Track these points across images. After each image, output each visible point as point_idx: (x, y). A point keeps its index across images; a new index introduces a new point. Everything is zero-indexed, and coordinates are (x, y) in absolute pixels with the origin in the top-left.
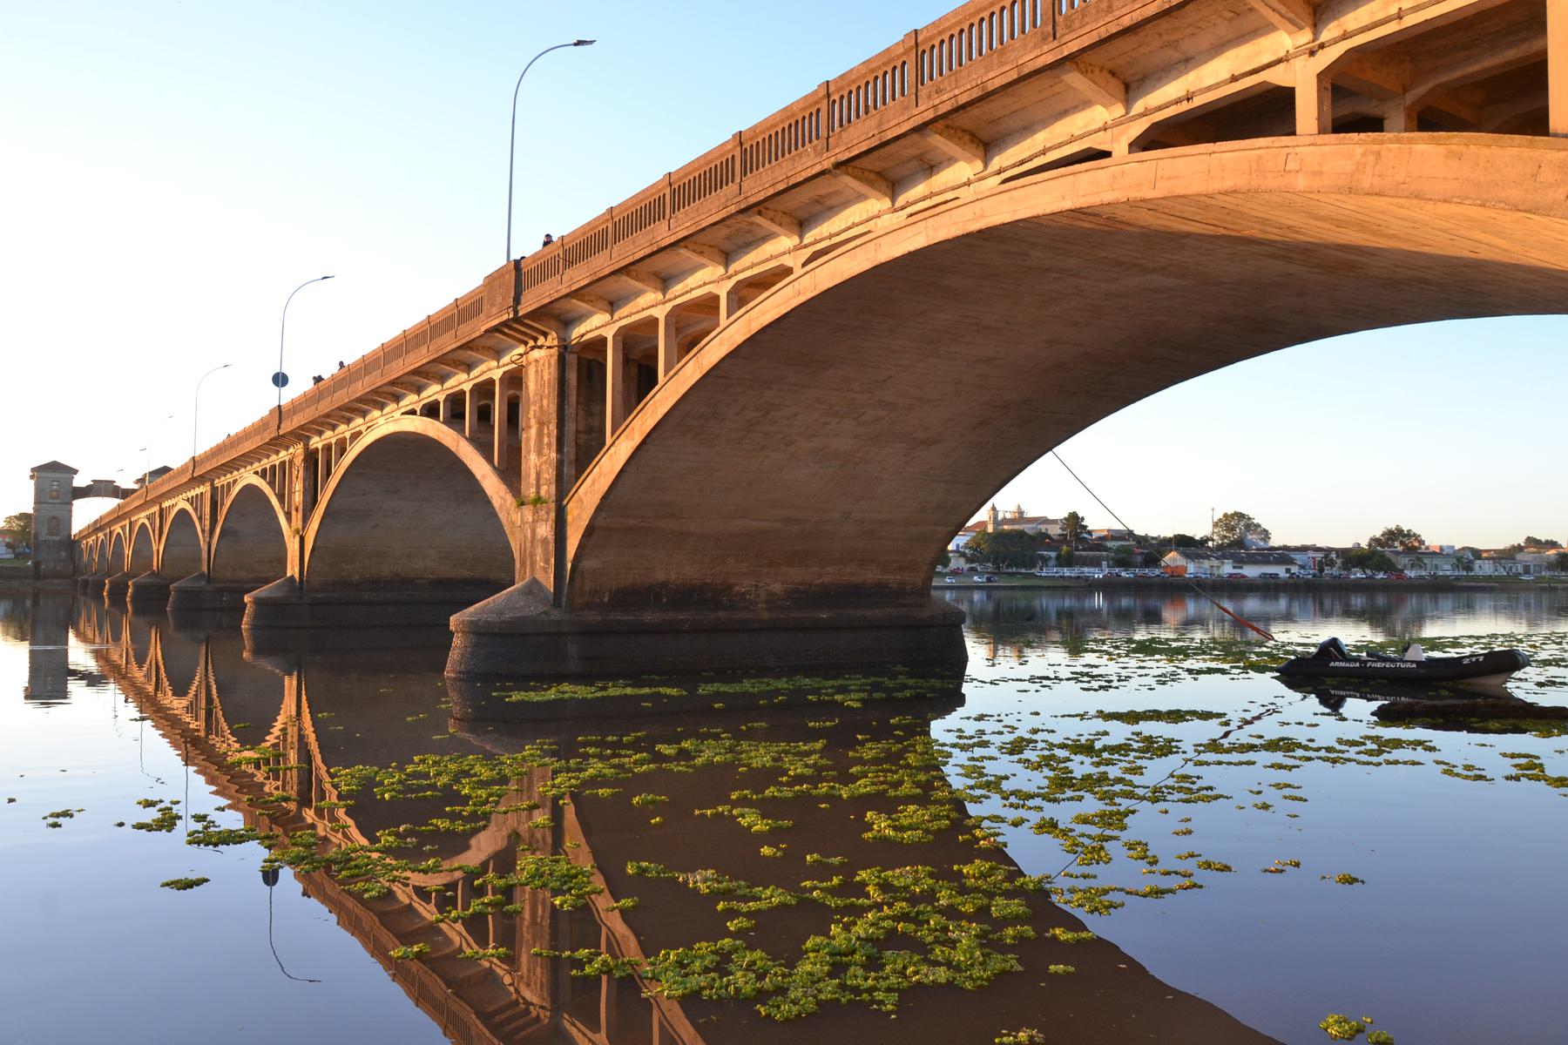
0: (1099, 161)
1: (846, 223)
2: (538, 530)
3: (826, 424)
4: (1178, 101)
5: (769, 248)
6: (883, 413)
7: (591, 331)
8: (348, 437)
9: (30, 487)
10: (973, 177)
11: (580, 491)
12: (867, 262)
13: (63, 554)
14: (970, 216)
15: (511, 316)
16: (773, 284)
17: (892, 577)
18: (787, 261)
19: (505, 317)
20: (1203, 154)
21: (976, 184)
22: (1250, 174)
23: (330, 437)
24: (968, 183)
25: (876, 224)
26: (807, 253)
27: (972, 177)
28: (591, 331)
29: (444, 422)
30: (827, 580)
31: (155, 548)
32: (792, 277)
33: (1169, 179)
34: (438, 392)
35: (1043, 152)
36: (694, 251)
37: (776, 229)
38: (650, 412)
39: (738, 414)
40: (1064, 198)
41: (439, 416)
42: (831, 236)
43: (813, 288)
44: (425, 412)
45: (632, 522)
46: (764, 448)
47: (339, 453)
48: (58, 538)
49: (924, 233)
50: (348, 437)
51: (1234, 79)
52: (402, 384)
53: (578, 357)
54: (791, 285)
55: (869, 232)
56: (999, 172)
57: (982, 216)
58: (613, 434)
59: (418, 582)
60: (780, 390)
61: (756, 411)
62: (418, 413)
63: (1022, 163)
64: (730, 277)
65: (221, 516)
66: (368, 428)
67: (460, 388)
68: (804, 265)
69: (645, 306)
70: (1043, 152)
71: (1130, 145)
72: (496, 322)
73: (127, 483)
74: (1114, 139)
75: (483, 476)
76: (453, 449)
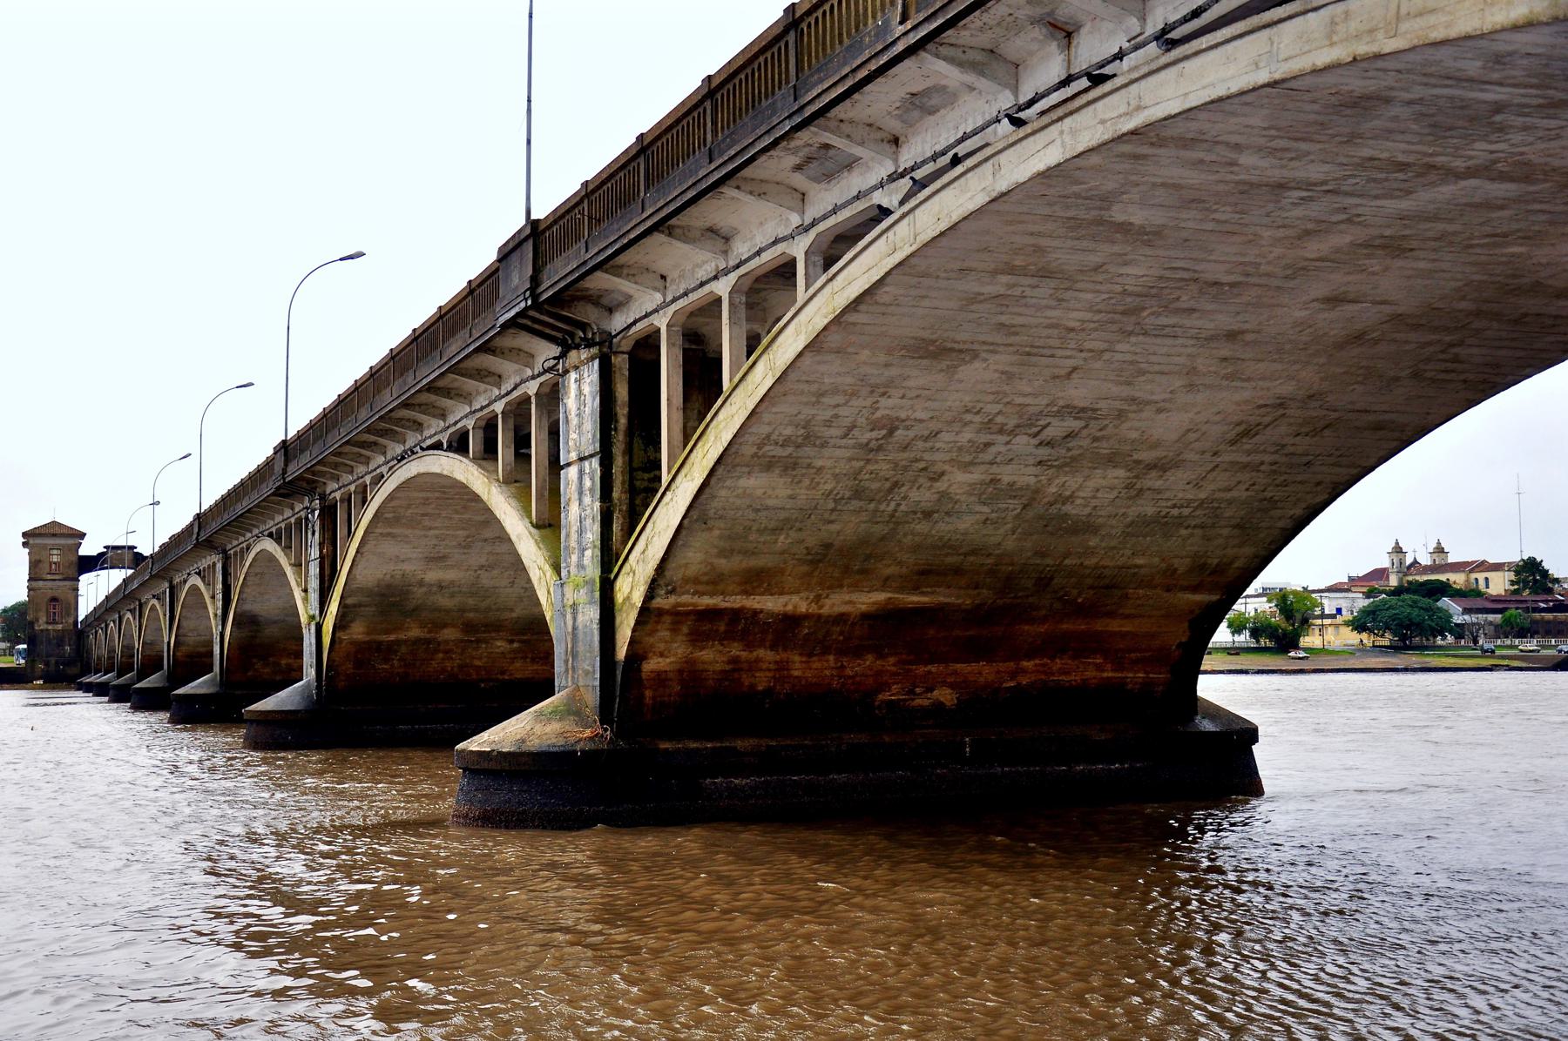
1: (956, 133)
2: (580, 618)
3: (987, 445)
5: (856, 182)
6: (1077, 424)
8: (470, 427)
10: (1128, 44)
11: (631, 557)
12: (981, 194)
14: (1123, 109)
16: (861, 237)
17: (1131, 675)
18: (879, 198)
19: (523, 305)
21: (1132, 55)
25: (995, 133)
27: (1126, 45)
29: (474, 460)
31: (166, 640)
33: (1420, 14)
36: (751, 193)
37: (857, 151)
38: (713, 439)
39: (845, 436)
40: (1257, 67)
41: (468, 452)
43: (912, 240)
44: (455, 444)
47: (679, 437)
48: (60, 627)
49: (1058, 142)
50: (470, 427)
52: (420, 405)
54: (885, 236)
55: (987, 145)
57: (1139, 108)
61: (872, 430)
62: (445, 446)
63: (1196, 14)
64: (806, 230)
65: (350, 534)
66: (390, 469)
68: (902, 203)
69: (704, 279)
75: (519, 536)
76: (485, 497)
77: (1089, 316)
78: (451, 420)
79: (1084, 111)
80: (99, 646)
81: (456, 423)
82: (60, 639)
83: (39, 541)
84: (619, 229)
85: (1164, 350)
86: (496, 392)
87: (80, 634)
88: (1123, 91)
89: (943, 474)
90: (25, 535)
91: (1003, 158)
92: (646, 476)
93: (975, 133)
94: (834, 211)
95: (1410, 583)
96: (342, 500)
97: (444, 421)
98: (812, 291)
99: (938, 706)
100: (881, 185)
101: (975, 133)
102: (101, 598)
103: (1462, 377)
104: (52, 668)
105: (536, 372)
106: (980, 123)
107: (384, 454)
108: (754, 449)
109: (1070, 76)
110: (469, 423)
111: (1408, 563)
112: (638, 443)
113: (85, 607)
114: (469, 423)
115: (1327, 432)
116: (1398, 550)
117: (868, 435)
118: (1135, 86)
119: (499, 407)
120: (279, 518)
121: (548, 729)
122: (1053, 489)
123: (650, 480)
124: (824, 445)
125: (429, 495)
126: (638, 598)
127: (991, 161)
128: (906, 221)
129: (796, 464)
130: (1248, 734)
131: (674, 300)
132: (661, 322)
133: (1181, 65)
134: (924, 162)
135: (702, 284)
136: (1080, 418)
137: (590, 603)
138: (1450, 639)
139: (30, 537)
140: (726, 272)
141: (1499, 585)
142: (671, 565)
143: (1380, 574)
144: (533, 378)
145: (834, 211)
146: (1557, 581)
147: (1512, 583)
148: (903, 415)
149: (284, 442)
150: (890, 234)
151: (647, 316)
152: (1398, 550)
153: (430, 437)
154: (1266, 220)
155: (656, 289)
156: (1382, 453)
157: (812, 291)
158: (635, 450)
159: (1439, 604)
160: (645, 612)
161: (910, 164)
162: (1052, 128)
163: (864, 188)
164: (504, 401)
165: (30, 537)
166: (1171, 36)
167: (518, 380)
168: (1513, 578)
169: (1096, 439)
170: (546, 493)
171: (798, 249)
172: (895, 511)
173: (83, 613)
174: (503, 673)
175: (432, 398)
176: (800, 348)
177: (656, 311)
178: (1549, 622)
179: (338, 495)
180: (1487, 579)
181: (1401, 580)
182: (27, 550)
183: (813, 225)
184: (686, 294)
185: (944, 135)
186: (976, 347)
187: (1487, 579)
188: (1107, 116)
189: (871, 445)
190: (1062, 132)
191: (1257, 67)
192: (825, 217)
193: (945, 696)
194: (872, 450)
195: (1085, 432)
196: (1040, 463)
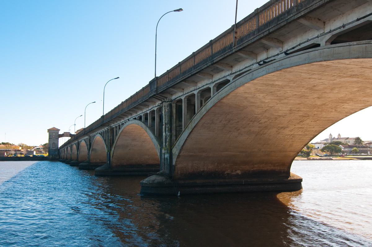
0: (316, 48)
2: (165, 156)
4: (340, 28)
7: (178, 97)
8: (142, 115)
9: (47, 135)
13: (56, 153)
15: (156, 93)
17: (277, 168)
18: (228, 78)
19: (154, 94)
20: (348, 46)
22: (363, 52)
23: (193, 89)
24: (278, 55)
25: (252, 67)
26: (234, 76)
27: (279, 53)
28: (178, 97)
29: (143, 122)
30: (255, 169)
32: (229, 83)
34: (141, 113)
35: (299, 45)
39: (220, 122)
42: (240, 71)
45: (191, 154)
46: (230, 131)
48: (55, 148)
49: (265, 70)
51: (358, 20)
53: (176, 104)
55: (251, 70)
56: (330, 32)
58: (184, 128)
59: (143, 165)
60: (232, 115)
63: (293, 48)
64: (213, 83)
66: (125, 122)
67: (147, 112)
70: (299, 45)
71: (326, 42)
72: (152, 95)
73: (73, 133)
74: (321, 40)
77: (270, 100)
78: (138, 114)
79: (270, 65)
80: (62, 155)
81: (139, 114)
82: (55, 150)
83: (51, 131)
84: (175, 80)
85: (285, 106)
86: (148, 109)
87: (59, 150)
88: (279, 62)
89: (240, 129)
90: (48, 130)
91: (254, 73)
92: (179, 128)
93: (248, 67)
94: (219, 79)
95: (333, 142)
96: (115, 127)
97: (142, 111)
98: (214, 95)
99: (238, 174)
100: (229, 75)
101: (248, 67)
102: (63, 143)
103: (345, 111)
104: (53, 157)
105: (156, 106)
106: (249, 65)
107: (124, 119)
108: (202, 125)
109: (268, 57)
110: (142, 115)
111: (333, 138)
112: (177, 121)
113: (60, 145)
114: (142, 115)
115: (318, 121)
116: (331, 135)
117: (225, 122)
118: (281, 61)
119: (148, 112)
120: (101, 130)
121: (159, 178)
122: (262, 132)
123: (180, 129)
124: (216, 124)
125: (133, 128)
126: (177, 153)
127: (251, 73)
128: (233, 83)
129: (210, 127)
130: (301, 180)
131: (185, 94)
132: (183, 98)
133: (290, 58)
134: (238, 72)
135: (191, 91)
136: (267, 119)
137: (168, 153)
138: (341, 154)
139: (49, 131)
140: (196, 89)
141: (351, 143)
142: (184, 147)
143: (326, 140)
144: (156, 107)
145: (219, 79)
146: (363, 142)
147: (354, 142)
148: (232, 118)
149: (103, 116)
150: (231, 85)
151: (180, 96)
152: (331, 135)
153: (134, 117)
154: (306, 84)
155: (182, 92)
156: (329, 125)
157: (214, 95)
158: (177, 123)
159: (339, 146)
160: (179, 156)
161: (235, 72)
162: (264, 67)
163: (225, 75)
164: (149, 111)
165: (49, 131)
166: (287, 52)
167: (152, 107)
168: (355, 141)
169: (270, 123)
170: (158, 130)
171: (211, 86)
172: (230, 136)
173: (59, 147)
174: (147, 162)
175: (134, 109)
176: (212, 106)
177: (181, 96)
178: (361, 150)
179: (114, 127)
180: (349, 141)
181: (331, 141)
182: (48, 133)
183: (215, 81)
184: (188, 93)
185: (242, 67)
186: (247, 106)
187: (349, 141)
188: (275, 66)
189: (225, 124)
190: (266, 69)
191: (306, 60)
192: (217, 80)
193: (239, 172)
194: (225, 125)
195: (268, 122)
196: (259, 127)
